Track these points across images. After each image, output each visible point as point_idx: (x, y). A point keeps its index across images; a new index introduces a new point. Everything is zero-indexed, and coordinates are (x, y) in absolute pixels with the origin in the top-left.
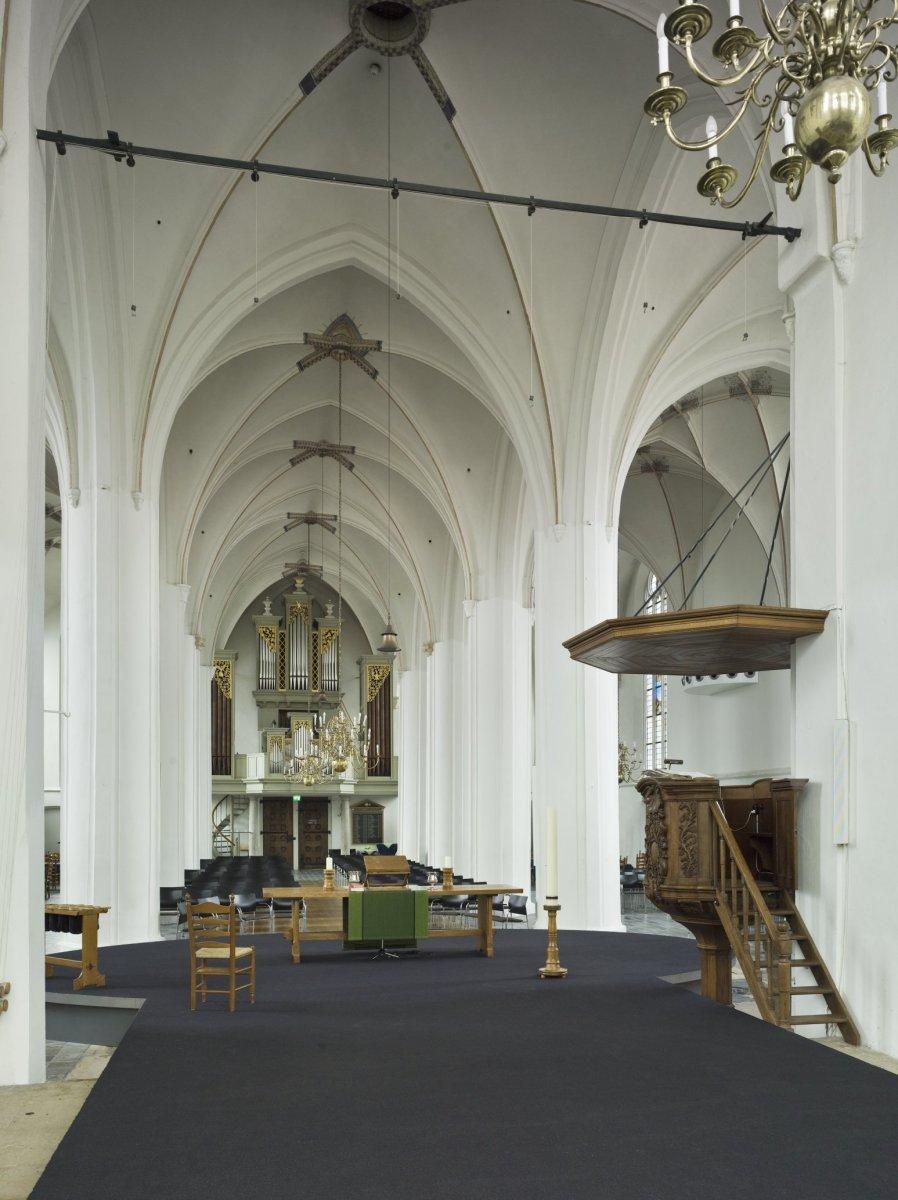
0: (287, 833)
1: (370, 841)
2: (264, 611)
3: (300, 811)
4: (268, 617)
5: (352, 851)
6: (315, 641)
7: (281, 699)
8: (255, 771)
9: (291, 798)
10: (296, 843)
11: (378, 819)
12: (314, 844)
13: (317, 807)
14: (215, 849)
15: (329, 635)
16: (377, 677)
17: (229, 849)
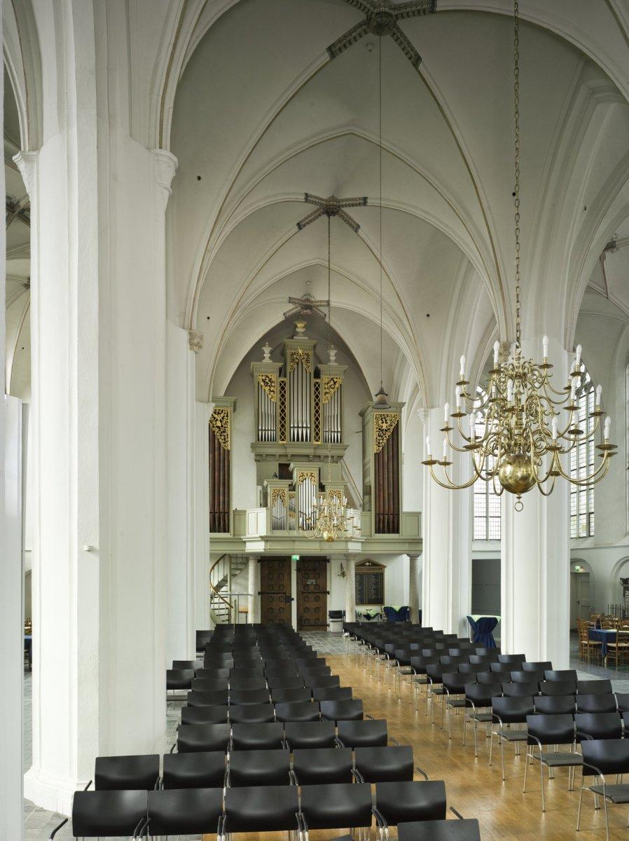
0: (285, 593)
1: (371, 602)
2: (264, 358)
3: (298, 570)
4: (267, 365)
5: (358, 615)
6: (317, 389)
7: (281, 451)
8: (254, 528)
9: (289, 558)
10: (294, 604)
11: (379, 578)
12: (313, 605)
13: (315, 567)
14: (213, 618)
15: (332, 383)
16: (384, 426)
17: (227, 612)
